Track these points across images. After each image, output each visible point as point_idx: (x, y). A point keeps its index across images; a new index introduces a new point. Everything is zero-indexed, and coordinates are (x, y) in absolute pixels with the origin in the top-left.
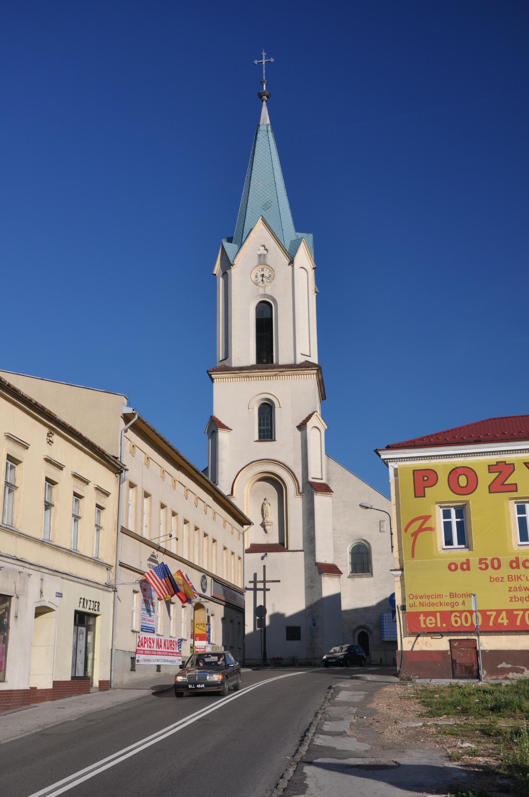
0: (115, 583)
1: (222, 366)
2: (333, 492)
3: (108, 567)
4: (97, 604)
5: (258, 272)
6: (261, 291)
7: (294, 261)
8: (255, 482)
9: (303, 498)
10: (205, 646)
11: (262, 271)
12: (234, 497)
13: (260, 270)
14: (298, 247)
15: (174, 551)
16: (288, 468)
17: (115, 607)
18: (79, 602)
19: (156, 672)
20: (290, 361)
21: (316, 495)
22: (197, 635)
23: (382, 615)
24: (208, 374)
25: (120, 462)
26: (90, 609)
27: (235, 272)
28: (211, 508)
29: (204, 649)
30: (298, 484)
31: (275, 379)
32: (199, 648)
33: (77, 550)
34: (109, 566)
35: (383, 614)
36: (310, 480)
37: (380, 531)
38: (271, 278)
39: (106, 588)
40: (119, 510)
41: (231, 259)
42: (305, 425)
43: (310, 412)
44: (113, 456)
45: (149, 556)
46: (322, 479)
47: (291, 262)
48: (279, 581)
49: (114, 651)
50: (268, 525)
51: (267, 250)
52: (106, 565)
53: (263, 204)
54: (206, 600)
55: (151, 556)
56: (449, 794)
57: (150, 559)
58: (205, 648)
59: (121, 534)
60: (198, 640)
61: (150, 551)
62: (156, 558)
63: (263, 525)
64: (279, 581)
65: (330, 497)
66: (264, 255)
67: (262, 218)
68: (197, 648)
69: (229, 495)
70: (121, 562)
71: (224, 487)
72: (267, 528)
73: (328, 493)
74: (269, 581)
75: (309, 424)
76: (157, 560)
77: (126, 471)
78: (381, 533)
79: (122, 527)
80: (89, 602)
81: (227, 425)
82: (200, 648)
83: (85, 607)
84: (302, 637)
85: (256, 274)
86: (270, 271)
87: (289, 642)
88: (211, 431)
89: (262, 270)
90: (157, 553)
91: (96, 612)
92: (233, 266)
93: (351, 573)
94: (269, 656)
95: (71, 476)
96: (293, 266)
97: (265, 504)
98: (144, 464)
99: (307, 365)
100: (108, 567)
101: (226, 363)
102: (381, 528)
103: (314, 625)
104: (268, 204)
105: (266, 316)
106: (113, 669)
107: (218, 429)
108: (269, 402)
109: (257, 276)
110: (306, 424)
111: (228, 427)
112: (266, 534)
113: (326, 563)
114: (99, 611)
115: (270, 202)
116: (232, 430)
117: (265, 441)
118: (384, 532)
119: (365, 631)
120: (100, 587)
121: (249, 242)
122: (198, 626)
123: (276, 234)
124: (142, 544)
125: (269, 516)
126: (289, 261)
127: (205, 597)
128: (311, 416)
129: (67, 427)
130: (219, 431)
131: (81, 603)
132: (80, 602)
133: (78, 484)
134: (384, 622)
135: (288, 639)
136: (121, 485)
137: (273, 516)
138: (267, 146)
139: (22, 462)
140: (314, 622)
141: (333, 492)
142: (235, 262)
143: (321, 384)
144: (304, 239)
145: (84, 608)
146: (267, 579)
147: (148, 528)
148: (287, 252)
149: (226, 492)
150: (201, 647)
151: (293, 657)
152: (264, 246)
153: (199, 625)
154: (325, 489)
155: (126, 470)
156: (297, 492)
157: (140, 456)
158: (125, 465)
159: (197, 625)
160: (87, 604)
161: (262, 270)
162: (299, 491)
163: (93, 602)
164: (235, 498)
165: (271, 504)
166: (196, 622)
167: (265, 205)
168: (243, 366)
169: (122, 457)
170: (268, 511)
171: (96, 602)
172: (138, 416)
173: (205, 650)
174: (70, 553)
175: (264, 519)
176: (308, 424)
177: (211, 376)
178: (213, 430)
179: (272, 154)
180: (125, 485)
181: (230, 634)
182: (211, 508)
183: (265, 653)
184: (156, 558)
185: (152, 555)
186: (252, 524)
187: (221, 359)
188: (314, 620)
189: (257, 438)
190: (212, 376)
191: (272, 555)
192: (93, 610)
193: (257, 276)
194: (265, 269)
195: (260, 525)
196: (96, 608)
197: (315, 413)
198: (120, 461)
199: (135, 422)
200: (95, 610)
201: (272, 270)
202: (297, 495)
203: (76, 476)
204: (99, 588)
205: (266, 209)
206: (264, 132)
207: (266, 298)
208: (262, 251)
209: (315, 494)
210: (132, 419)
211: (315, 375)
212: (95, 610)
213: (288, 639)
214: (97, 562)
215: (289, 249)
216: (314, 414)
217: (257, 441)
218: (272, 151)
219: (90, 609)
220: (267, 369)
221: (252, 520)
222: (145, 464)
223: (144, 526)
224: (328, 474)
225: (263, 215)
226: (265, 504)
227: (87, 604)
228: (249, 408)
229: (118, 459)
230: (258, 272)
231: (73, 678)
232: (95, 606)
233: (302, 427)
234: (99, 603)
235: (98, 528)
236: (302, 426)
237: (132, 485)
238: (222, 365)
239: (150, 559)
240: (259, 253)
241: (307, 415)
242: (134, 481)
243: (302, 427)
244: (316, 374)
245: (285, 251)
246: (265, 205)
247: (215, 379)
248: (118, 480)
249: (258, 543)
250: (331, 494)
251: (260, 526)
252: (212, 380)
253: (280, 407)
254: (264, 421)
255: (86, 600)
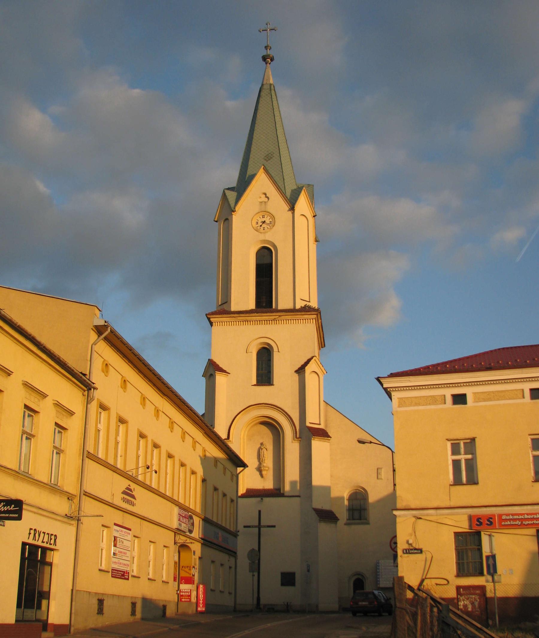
0: (78, 514)
1: (221, 310)
2: (331, 437)
3: (70, 497)
4: (53, 537)
5: (259, 219)
6: (262, 237)
7: (295, 208)
8: (252, 426)
9: (300, 443)
10: (190, 590)
11: (263, 218)
12: (231, 441)
13: (261, 217)
14: (299, 195)
15: (154, 485)
16: (286, 413)
17: (78, 543)
18: (29, 532)
19: (130, 617)
20: (290, 306)
21: (314, 440)
22: (182, 578)
23: (378, 561)
24: (207, 317)
25: (89, 380)
26: (43, 542)
27: (236, 219)
28: (201, 445)
29: (190, 593)
30: (296, 429)
31: (274, 324)
32: (185, 592)
33: (28, 473)
34: (70, 495)
35: (379, 561)
36: (308, 424)
37: (313, 185)
38: (273, 224)
39: (66, 520)
40: (86, 434)
41: (232, 205)
42: (303, 370)
43: (309, 357)
44: (81, 373)
45: (123, 489)
46: (320, 424)
47: (292, 209)
48: (274, 526)
49: (74, 592)
50: (265, 470)
51: (268, 198)
52: (67, 494)
53: (265, 155)
54: (191, 541)
55: (126, 489)
56: (200, 601)
57: (124, 493)
58: (190, 592)
59: (87, 460)
60: (183, 583)
61: (125, 483)
62: (133, 492)
63: (259, 470)
64: (274, 526)
65: (328, 443)
66: (265, 202)
67: (263, 168)
68: (182, 592)
69: (225, 439)
70: (86, 492)
71: (221, 430)
72: (264, 473)
73: (326, 438)
74: (265, 527)
75: (308, 369)
76: (133, 494)
77: (95, 390)
78: (378, 481)
79: (89, 452)
80: (42, 535)
81: (224, 368)
82: (186, 592)
83: (37, 539)
84: (297, 584)
85: (257, 221)
86: (271, 218)
87: (284, 588)
88: (209, 374)
89: (263, 217)
90: (133, 486)
91: (52, 547)
92: (234, 212)
93: (347, 520)
94: (263, 601)
95: (22, 386)
96: (293, 213)
97: (262, 449)
98: (120, 386)
99: (306, 309)
100: (70, 497)
101: (225, 307)
102: (379, 475)
103: (308, 571)
104: (270, 155)
105: (266, 261)
106: (73, 611)
107: (216, 372)
108: (267, 347)
109: (257, 222)
110: (305, 368)
111: (226, 371)
112: (262, 479)
113: (323, 509)
114: (56, 545)
115: (272, 153)
116: (230, 374)
117: (262, 385)
118: (382, 479)
119: (360, 577)
120: (59, 518)
121: (250, 189)
122: (183, 568)
123: (278, 182)
124: (115, 473)
125: (266, 461)
126: (289, 207)
127: (190, 538)
128: (310, 361)
129: (16, 326)
130: (216, 374)
131: (31, 535)
132: (30, 534)
133: (32, 397)
134: (380, 568)
135: (283, 584)
136: (89, 405)
137: (269, 462)
138: (270, 102)
139: (122, 493)
140: (308, 568)
141: (331, 437)
142: (237, 209)
143: (320, 330)
144: (304, 188)
145: (35, 540)
146: (262, 524)
147: (123, 457)
148: (288, 200)
149: (223, 435)
150: (186, 591)
151: (287, 603)
152: (265, 194)
153: (185, 567)
154: (323, 434)
155: (95, 388)
156: (295, 437)
157: (114, 379)
158: (94, 383)
159: (182, 567)
160: (39, 536)
161: (263, 217)
162: (296, 436)
163: (48, 534)
164: (231, 442)
165: (267, 449)
166: (181, 564)
167: (267, 156)
168: (242, 310)
169: (91, 374)
170: (265, 456)
171: (52, 535)
172: (111, 329)
173: (190, 594)
174: (17, 474)
175: (260, 464)
176: (306, 368)
177: (210, 319)
178: (211, 373)
179: (275, 110)
180: (94, 406)
181: (221, 579)
182: (201, 445)
183: (258, 599)
184: (133, 492)
185: (127, 488)
186: (246, 466)
187: (220, 304)
188: (308, 566)
189: (255, 382)
190: (211, 319)
191: (267, 500)
192: (47, 543)
193: (257, 222)
194: (266, 216)
195: (255, 468)
196: (52, 542)
197: (314, 358)
198: (88, 378)
199: (107, 335)
200: (51, 544)
201: (273, 217)
202: (294, 440)
203: (27, 385)
204: (56, 520)
205: (267, 159)
206: (268, 91)
207: (267, 244)
208: (264, 199)
209: (312, 439)
210: (104, 333)
211: (314, 320)
212: (51, 544)
213: (283, 584)
214: (54, 489)
215: (290, 197)
216: (312, 359)
217: (255, 385)
218: (274, 107)
219: (43, 542)
220: (266, 313)
221: (246, 461)
222: (122, 387)
223: (119, 456)
224: (326, 421)
225: (265, 165)
226: (262, 449)
227: (39, 536)
228: (248, 352)
229: (86, 376)
230: (259, 219)
231: (16, 621)
232: (51, 539)
233: (301, 371)
234: (55, 536)
235: (59, 451)
236: (300, 371)
237: (103, 407)
238: (221, 309)
239: (124, 493)
240: (260, 200)
241: (305, 360)
242: (106, 403)
243: (301, 371)
244: (315, 319)
245: (286, 198)
246: (267, 156)
247: (214, 323)
248: (85, 399)
249: (254, 488)
250: (329, 440)
251: (256, 470)
252: (211, 324)
253: (279, 352)
254: (263, 365)
255: (39, 531)
